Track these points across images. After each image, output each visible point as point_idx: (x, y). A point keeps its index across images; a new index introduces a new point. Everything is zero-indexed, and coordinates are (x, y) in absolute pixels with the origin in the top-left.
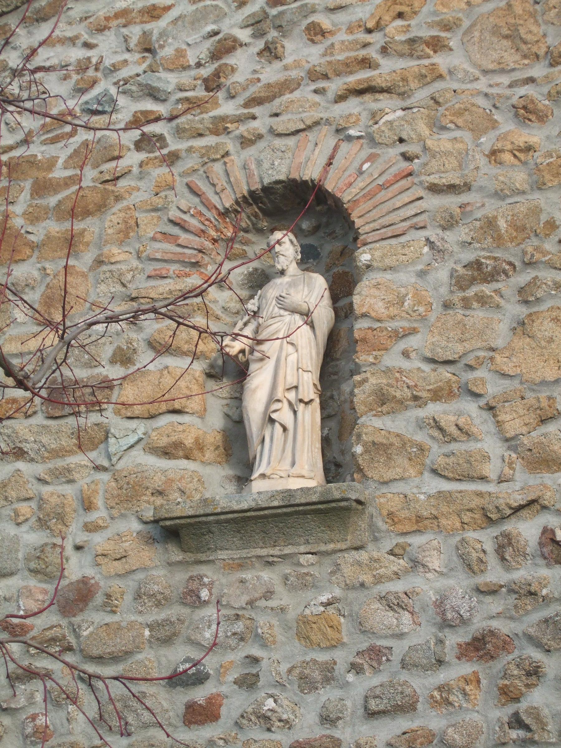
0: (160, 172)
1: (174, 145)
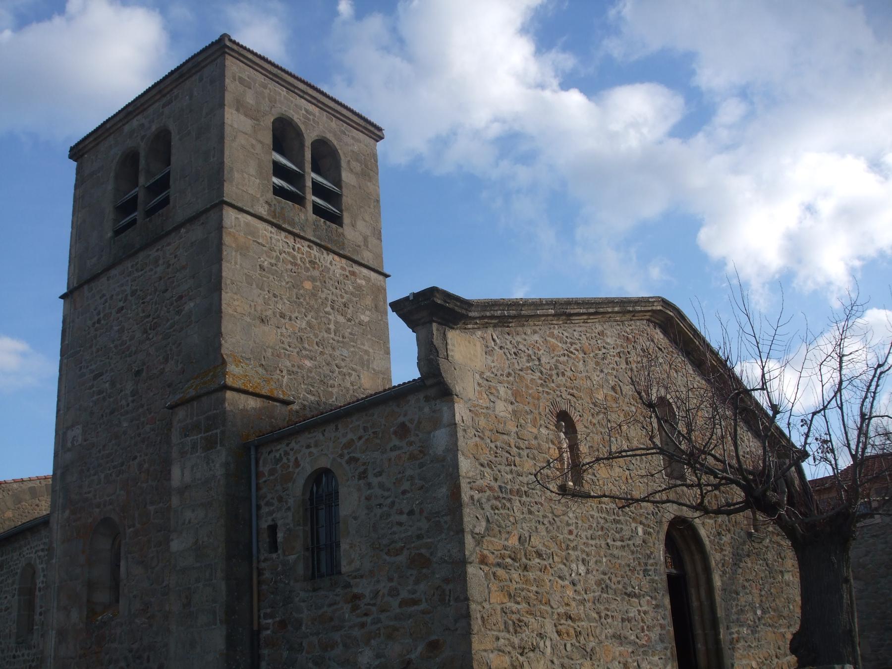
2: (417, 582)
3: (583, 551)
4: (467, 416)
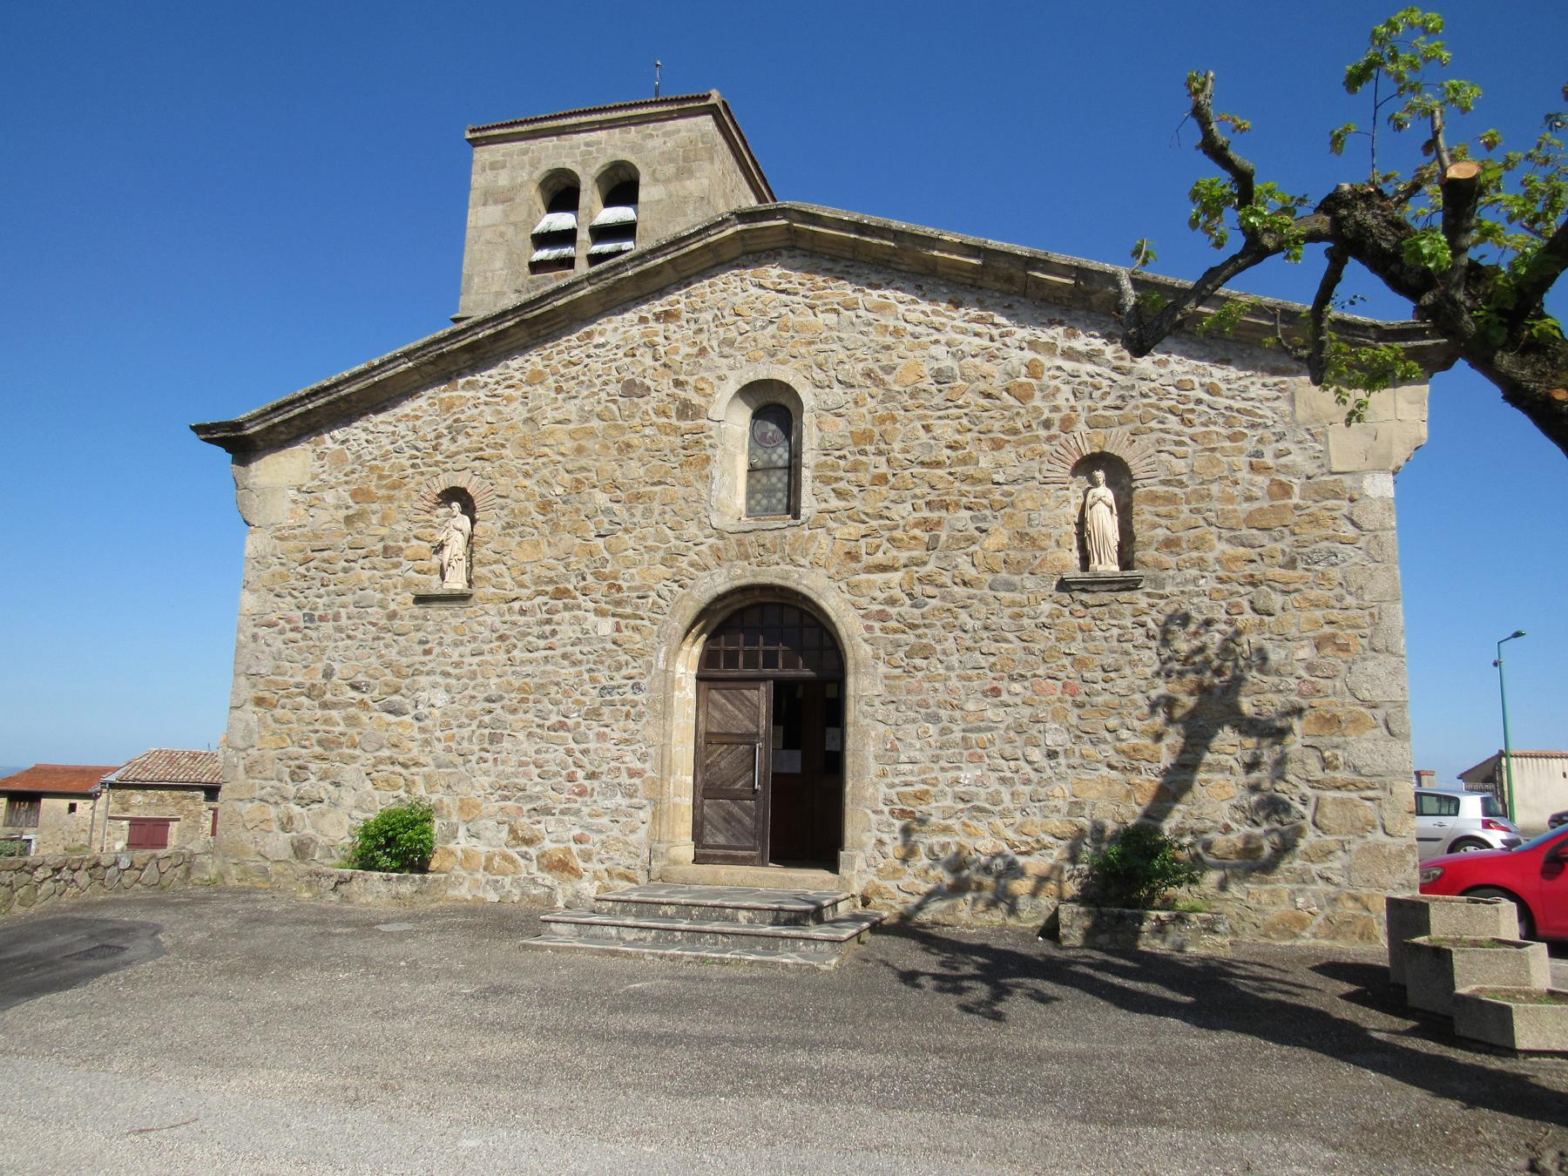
0: (418, 478)
1: (423, 469)
3: (446, 674)
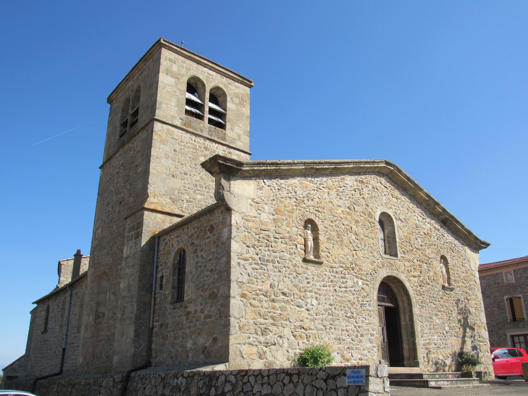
2: (211, 306)
3: (316, 293)
4: (241, 222)
